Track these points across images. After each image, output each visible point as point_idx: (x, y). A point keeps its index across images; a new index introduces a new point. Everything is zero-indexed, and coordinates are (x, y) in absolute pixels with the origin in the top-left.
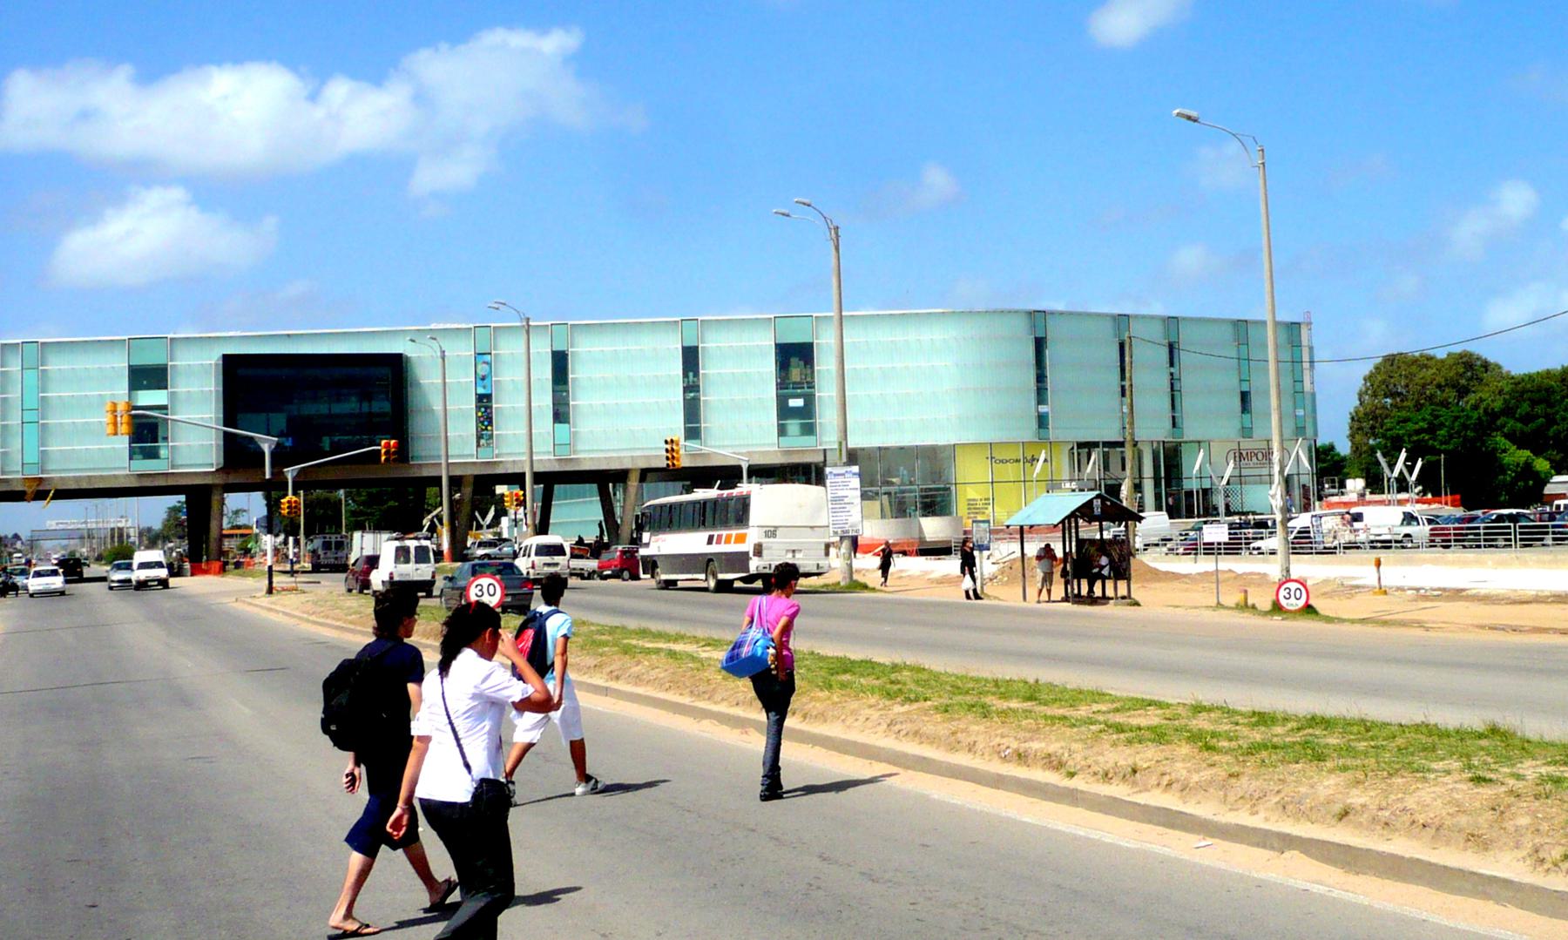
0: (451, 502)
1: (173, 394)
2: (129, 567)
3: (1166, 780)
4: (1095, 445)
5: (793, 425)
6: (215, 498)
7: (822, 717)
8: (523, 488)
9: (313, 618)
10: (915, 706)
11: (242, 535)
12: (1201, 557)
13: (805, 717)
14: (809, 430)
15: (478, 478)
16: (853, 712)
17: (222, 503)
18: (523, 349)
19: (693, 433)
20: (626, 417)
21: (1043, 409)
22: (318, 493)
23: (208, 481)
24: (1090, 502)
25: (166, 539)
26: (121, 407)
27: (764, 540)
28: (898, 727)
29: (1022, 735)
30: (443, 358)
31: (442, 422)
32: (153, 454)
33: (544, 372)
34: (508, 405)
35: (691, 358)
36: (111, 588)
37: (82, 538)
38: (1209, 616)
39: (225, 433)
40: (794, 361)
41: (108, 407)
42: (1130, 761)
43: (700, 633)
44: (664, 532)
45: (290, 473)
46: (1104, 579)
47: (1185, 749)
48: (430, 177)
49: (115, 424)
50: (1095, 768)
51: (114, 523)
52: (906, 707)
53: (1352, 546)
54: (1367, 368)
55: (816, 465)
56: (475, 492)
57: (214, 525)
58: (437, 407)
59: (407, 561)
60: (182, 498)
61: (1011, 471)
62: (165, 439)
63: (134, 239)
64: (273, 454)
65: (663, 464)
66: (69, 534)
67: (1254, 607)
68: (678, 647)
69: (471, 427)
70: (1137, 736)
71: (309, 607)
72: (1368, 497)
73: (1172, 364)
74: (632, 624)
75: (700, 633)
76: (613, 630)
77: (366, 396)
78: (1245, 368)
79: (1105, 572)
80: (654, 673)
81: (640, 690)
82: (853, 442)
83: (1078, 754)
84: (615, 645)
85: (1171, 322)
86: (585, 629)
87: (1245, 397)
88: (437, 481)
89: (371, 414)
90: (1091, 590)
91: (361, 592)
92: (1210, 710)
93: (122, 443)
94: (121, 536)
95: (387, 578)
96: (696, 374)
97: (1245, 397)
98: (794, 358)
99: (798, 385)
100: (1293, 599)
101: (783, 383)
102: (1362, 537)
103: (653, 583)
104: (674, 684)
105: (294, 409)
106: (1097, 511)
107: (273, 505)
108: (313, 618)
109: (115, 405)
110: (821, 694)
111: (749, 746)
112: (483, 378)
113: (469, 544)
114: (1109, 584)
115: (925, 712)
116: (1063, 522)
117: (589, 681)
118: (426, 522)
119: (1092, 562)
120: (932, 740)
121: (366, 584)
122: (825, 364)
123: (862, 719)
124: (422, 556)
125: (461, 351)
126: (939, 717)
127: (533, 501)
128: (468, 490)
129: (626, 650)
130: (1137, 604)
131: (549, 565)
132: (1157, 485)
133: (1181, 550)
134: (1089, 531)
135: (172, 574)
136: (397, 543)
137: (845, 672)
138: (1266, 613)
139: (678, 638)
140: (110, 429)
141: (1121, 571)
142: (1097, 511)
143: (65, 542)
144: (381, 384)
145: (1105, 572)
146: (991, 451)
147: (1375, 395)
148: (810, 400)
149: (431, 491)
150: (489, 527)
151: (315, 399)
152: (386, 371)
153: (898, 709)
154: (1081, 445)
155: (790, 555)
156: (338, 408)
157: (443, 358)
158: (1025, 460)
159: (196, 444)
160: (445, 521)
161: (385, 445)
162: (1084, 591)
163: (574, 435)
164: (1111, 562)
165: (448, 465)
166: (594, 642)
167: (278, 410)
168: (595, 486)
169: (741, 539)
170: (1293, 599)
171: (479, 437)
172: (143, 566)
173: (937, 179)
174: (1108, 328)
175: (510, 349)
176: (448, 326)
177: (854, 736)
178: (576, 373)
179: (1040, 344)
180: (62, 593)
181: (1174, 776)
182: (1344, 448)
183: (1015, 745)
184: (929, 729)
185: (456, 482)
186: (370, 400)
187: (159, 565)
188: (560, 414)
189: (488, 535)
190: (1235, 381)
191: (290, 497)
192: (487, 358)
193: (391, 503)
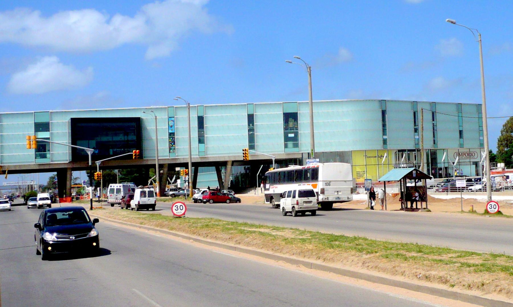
0: (160, 174)
1: (52, 133)
2: (35, 200)
3: (498, 289)
4: (405, 150)
5: (290, 144)
6: (69, 173)
7: (332, 260)
8: (188, 168)
9: (109, 219)
10: (372, 255)
11: (78, 187)
12: (449, 193)
13: (324, 260)
14: (296, 146)
15: (170, 165)
16: (346, 258)
17: (71, 175)
18: (187, 115)
19: (252, 147)
20: (227, 142)
21: (385, 137)
22: (108, 171)
23: (66, 166)
24: (412, 172)
25: (49, 189)
26: (32, 138)
27: (325, 187)
28: (367, 265)
29: (425, 268)
30: (156, 119)
31: (156, 145)
32: (44, 156)
33: (195, 124)
34: (181, 137)
35: (251, 118)
36: (29, 208)
37: (17, 189)
38: (460, 215)
39: (72, 147)
40: (290, 119)
41: (27, 138)
42: (480, 280)
43: (270, 224)
44: (276, 184)
45: (98, 163)
46: (416, 201)
47: (502, 275)
48: (152, 53)
49: (30, 144)
50: (464, 283)
51: (29, 183)
52: (368, 256)
53: (507, 188)
54: (504, 121)
55: (299, 159)
56: (168, 170)
57: (68, 183)
58: (154, 138)
59: (145, 197)
60: (56, 173)
61: (373, 161)
62: (49, 150)
63: (39, 76)
64: (92, 155)
65: (242, 159)
66: (12, 187)
67: (475, 212)
68: (262, 230)
69: (167, 145)
70: (480, 269)
71: (108, 214)
72: (506, 170)
73: (433, 120)
74: (240, 221)
75: (270, 224)
76: (233, 223)
77: (126, 134)
78: (461, 120)
79: (417, 199)
80: (255, 242)
81: (250, 248)
82: (317, 150)
83: (454, 277)
84: (236, 229)
85: (433, 104)
86: (221, 223)
87: (461, 132)
88: (154, 166)
89: (128, 141)
90: (412, 206)
91: (127, 208)
92: (500, 256)
93: (32, 152)
94: (32, 188)
95: (137, 203)
96: (253, 125)
97: (461, 132)
98: (290, 118)
99: (292, 129)
100: (493, 209)
101: (286, 128)
102: (509, 185)
103: (271, 205)
104: (264, 246)
105: (99, 139)
106: (414, 175)
107: (91, 176)
108: (109, 219)
109: (30, 137)
110: (330, 250)
111: (302, 272)
112: (171, 127)
113: (166, 190)
114: (419, 204)
115: (378, 258)
116: (400, 180)
117: (228, 244)
118: (149, 182)
119: (412, 196)
120: (384, 270)
121: (128, 206)
122: (303, 121)
123: (350, 261)
124: (151, 194)
125: (163, 116)
126: (384, 260)
127: (192, 173)
128: (166, 169)
129: (242, 232)
130: (430, 211)
131: (306, 202)
132: (428, 166)
133: (441, 190)
134: (410, 184)
135: (52, 202)
136: (141, 190)
137: (336, 240)
138: (482, 214)
139: (260, 226)
140: (28, 146)
141: (423, 198)
142: (414, 175)
143: (10, 190)
144: (131, 129)
145: (417, 199)
146: (366, 153)
147: (507, 132)
148: (296, 134)
149: (151, 170)
150: (173, 183)
151: (107, 135)
152: (134, 124)
153: (365, 256)
154: (399, 151)
155: (336, 193)
156: (117, 138)
157: (156, 119)
158: (378, 157)
159: (61, 152)
160: (157, 181)
161: (134, 152)
162: (409, 206)
163: (206, 148)
164: (420, 195)
165: (158, 159)
166: (226, 228)
167: (93, 139)
168: (214, 168)
169: (315, 186)
170: (493, 209)
171: (170, 149)
172: (41, 199)
173: (344, 53)
174: (409, 106)
175: (182, 115)
176: (158, 107)
177: (347, 268)
178: (207, 124)
179: (384, 113)
180: (10, 210)
181: (502, 287)
182: (495, 151)
183: (423, 273)
184: (381, 265)
185: (161, 166)
186: (128, 136)
187: (47, 199)
188: (201, 140)
189: (172, 186)
190: (457, 126)
191: (98, 172)
192: (173, 119)
193: (135, 175)
